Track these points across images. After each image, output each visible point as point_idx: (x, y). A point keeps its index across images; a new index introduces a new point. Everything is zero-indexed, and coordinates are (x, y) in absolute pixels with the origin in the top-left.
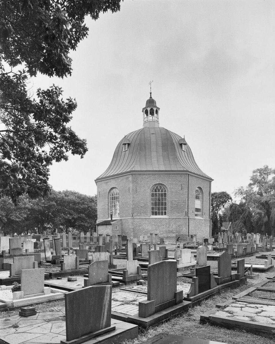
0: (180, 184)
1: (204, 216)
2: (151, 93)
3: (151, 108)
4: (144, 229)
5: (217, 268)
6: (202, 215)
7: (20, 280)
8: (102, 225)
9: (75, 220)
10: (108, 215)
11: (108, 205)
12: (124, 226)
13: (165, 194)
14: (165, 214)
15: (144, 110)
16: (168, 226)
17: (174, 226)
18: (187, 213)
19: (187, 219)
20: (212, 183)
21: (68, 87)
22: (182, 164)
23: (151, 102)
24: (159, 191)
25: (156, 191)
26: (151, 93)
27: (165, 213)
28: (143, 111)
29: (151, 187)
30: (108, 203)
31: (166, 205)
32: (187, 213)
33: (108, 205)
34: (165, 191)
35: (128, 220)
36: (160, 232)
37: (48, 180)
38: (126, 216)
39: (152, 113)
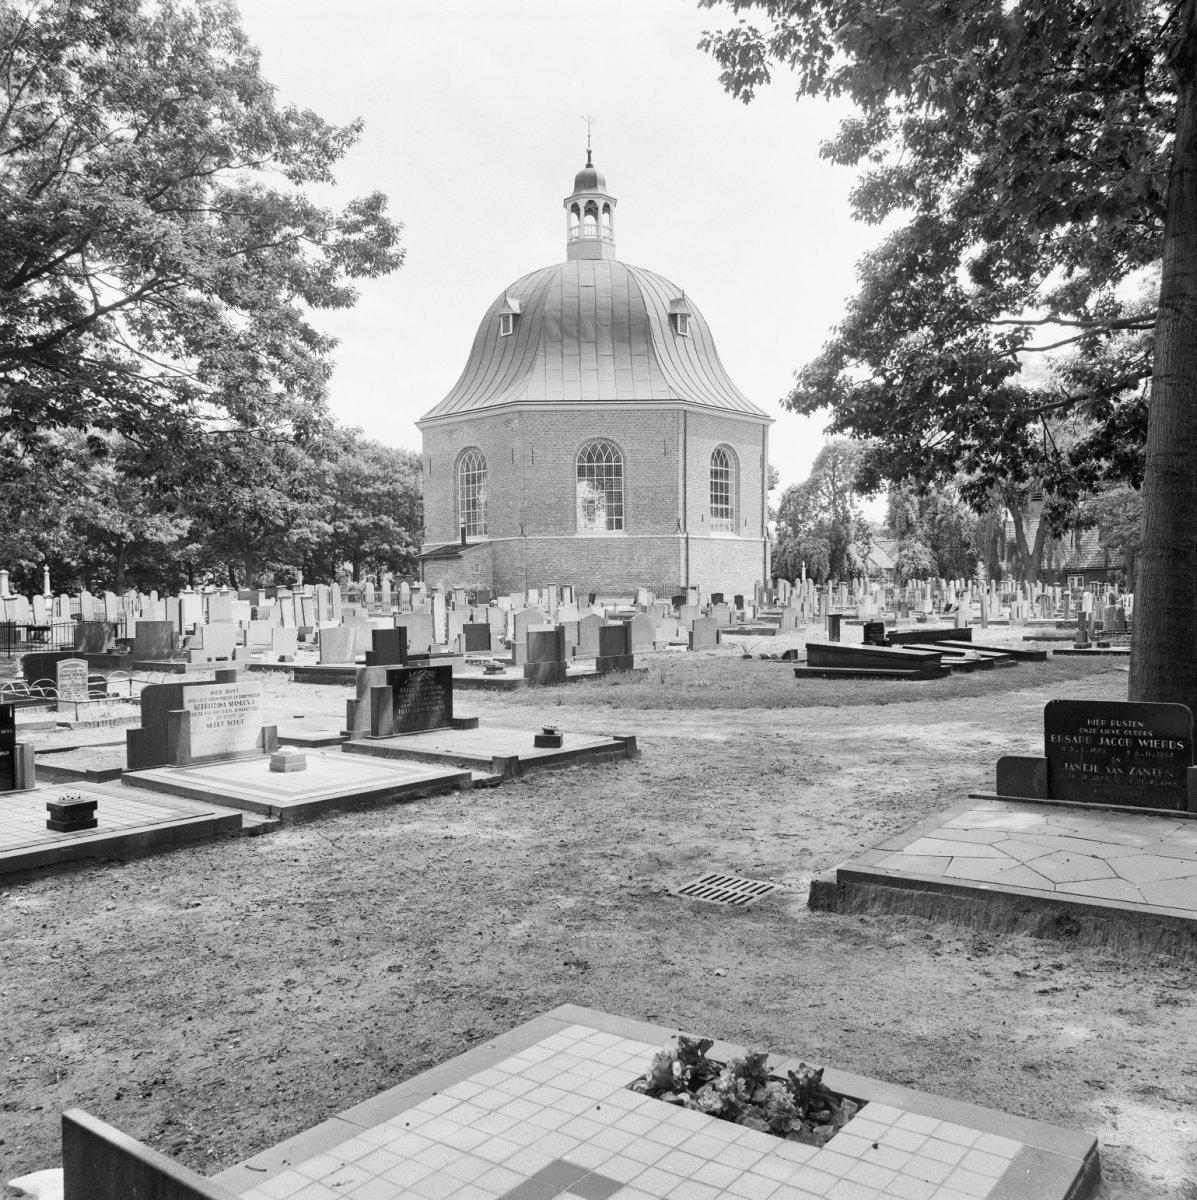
0: (659, 438)
1: (743, 530)
2: (589, 152)
3: (588, 195)
4: (556, 571)
5: (123, 743)
6: (736, 528)
7: (733, 1120)
8: (435, 559)
9: (362, 534)
10: (457, 529)
11: (455, 498)
12: (499, 562)
13: (618, 468)
14: (619, 526)
15: (569, 205)
16: (626, 561)
17: (643, 562)
18: (681, 522)
19: (683, 541)
20: (772, 429)
21: (320, 247)
22: (668, 378)
23: (587, 181)
24: (599, 459)
25: (590, 460)
26: (589, 152)
27: (619, 522)
28: (565, 206)
29: (575, 448)
30: (456, 492)
31: (620, 500)
32: (681, 522)
33: (455, 498)
34: (618, 460)
35: (513, 544)
36: (603, 579)
37: (335, 128)
38: (506, 533)
39: (591, 209)
